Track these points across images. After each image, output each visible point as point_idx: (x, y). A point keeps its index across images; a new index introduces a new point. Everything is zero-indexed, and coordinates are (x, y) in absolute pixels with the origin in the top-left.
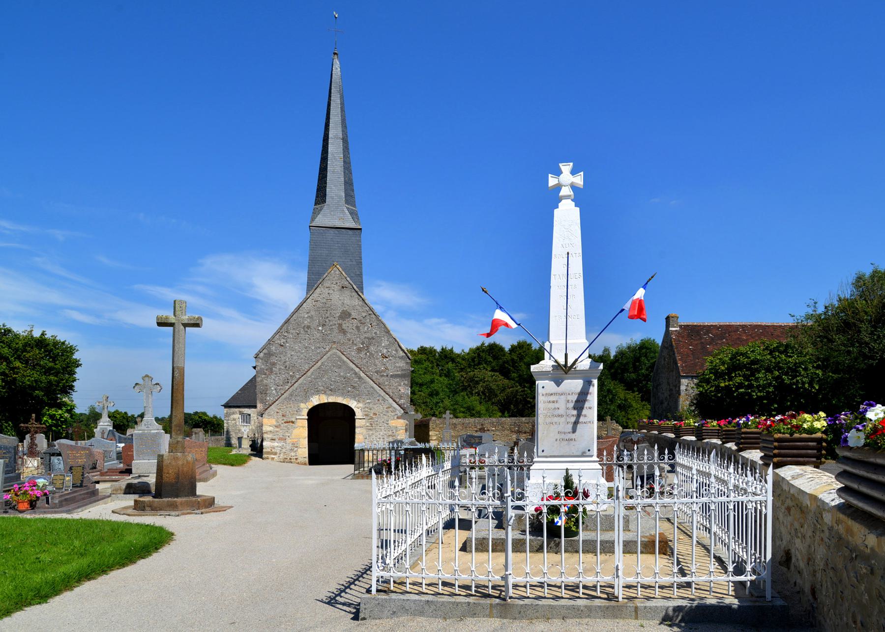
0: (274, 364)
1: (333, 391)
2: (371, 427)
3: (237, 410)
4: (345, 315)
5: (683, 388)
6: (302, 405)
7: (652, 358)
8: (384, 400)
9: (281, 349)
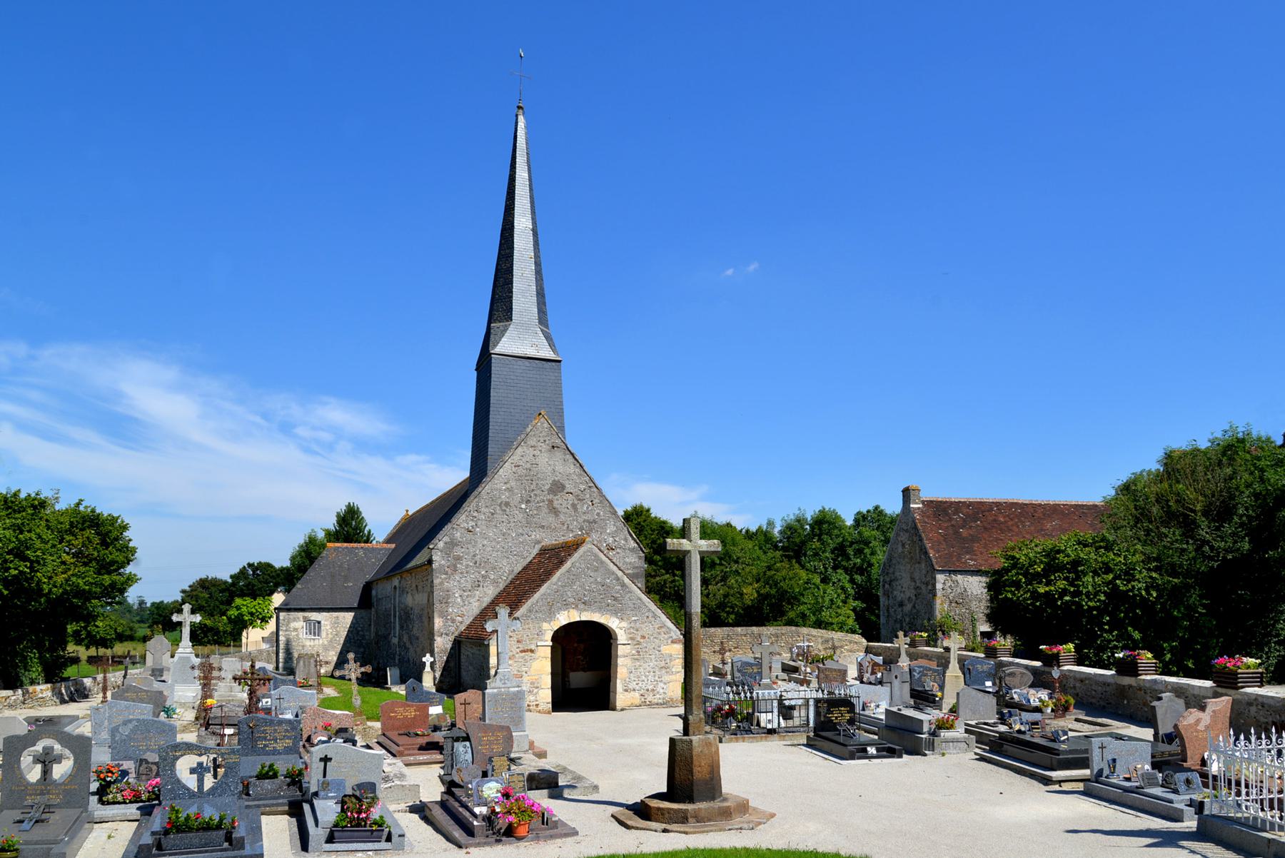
0: (458, 558)
1: (587, 604)
2: (638, 656)
3: (301, 614)
4: (557, 487)
5: (939, 586)
6: (545, 626)
7: (837, 536)
8: (655, 616)
9: (469, 536)
